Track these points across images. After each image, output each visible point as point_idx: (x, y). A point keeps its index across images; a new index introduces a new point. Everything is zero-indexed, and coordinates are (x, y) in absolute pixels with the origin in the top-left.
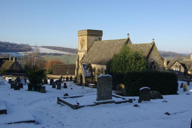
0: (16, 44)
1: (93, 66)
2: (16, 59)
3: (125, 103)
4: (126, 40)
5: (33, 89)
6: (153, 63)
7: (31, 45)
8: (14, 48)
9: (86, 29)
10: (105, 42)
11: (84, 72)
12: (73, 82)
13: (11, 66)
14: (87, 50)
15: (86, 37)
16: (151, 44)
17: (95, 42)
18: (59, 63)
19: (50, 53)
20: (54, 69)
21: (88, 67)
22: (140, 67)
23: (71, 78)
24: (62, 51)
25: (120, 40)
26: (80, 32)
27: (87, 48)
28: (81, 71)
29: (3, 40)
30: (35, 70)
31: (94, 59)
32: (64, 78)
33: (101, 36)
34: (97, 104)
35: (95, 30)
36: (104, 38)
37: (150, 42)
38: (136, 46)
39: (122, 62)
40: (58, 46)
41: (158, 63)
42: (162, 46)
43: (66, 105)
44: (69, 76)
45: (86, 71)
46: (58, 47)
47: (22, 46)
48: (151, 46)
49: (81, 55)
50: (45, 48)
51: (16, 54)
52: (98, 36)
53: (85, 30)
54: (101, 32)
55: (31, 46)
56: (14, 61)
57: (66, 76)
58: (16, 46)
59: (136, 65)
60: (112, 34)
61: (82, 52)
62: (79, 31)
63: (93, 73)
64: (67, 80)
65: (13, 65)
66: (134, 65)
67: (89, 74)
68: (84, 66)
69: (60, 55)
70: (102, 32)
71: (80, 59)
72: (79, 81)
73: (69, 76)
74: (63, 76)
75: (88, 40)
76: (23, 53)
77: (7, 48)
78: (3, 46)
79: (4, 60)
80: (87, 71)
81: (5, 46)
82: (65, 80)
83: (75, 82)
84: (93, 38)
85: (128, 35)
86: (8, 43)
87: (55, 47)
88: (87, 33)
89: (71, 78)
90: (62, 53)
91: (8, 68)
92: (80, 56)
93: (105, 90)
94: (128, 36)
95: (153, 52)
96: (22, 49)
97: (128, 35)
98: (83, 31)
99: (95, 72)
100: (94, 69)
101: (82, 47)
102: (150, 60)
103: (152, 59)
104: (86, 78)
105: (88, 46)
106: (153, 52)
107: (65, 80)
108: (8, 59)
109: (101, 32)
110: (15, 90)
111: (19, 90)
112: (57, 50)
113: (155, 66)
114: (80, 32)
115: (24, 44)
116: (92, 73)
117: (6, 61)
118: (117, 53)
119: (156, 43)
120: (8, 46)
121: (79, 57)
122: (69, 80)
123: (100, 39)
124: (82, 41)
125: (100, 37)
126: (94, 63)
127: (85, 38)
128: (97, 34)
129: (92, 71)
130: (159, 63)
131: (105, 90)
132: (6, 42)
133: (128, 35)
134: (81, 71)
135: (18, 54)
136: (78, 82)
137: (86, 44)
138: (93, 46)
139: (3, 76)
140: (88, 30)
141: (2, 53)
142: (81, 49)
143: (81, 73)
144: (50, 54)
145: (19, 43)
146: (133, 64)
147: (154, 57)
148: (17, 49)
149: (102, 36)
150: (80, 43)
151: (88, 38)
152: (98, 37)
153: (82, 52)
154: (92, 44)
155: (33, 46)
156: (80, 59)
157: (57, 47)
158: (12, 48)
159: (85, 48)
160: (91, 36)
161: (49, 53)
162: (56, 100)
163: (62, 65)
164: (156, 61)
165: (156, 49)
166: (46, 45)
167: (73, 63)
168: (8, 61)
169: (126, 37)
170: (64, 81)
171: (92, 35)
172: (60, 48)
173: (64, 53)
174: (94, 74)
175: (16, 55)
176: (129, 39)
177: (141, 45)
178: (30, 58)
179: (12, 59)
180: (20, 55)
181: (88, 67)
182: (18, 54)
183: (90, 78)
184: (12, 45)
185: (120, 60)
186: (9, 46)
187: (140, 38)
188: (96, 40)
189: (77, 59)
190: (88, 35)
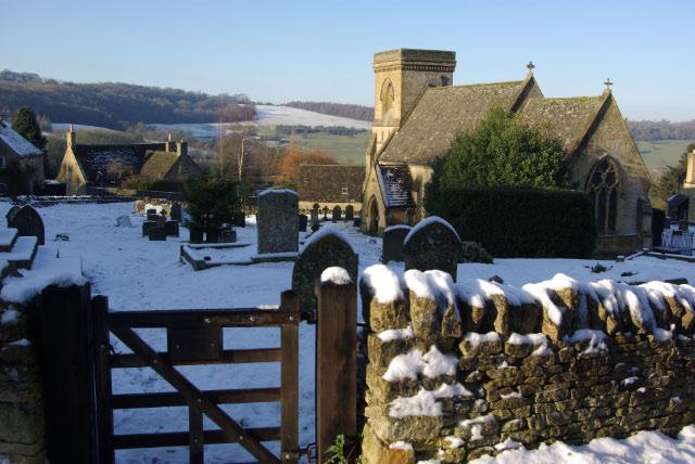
0: (204, 97)
1: (415, 171)
2: (184, 146)
3: (273, 264)
4: (520, 88)
5: (205, 239)
6: (604, 164)
7: (253, 99)
8: (197, 111)
9: (395, 48)
10: (457, 93)
11: (383, 190)
12: (352, 223)
13: (169, 172)
14: (402, 119)
15: (399, 71)
16: (601, 98)
17: (430, 91)
18: (323, 161)
19: (317, 127)
20: (301, 180)
21: (398, 175)
22: (533, 178)
23: (350, 209)
24: (361, 118)
25: (503, 85)
26: (379, 58)
27: (402, 110)
28: (375, 189)
29: (7, 75)
30: (206, 181)
31: (421, 148)
32: (326, 209)
33: (451, 70)
34: (256, 261)
35: (430, 52)
36: (460, 78)
37: (595, 91)
38: (552, 104)
39: (477, 158)
40: (344, 103)
41: (623, 163)
42: (634, 107)
43: (188, 263)
44: (343, 206)
45: (388, 188)
46: (347, 106)
47: (225, 101)
48: (599, 105)
49: (382, 133)
50: (301, 108)
51: (203, 128)
52: (440, 71)
53: (397, 51)
54: (449, 57)
55: (254, 103)
56: (179, 154)
57: (331, 206)
58: (203, 103)
59: (522, 169)
60: (482, 67)
61: (386, 124)
62: (376, 55)
63: (415, 195)
64: (336, 218)
65: (175, 166)
66: (513, 170)
67: (398, 198)
68: (384, 170)
69: (351, 132)
70: (454, 58)
71: (379, 147)
72: (368, 220)
73: (343, 206)
74: (322, 205)
75: (403, 85)
76: (226, 127)
77: (176, 110)
78: (162, 103)
79: (148, 152)
80: (394, 188)
81: (167, 102)
82: (330, 216)
83: (358, 223)
84: (422, 77)
85: (531, 66)
86: (180, 91)
87: (335, 104)
88: (399, 62)
89: (350, 209)
90: (347, 123)
91: (160, 177)
92: (379, 139)
93: (277, 228)
94: (528, 70)
95: (606, 126)
96: (226, 111)
97: (529, 66)
98: (387, 53)
99: (418, 191)
100: (417, 180)
101: (386, 107)
102: (593, 154)
103: (600, 152)
104: (389, 209)
105: (402, 103)
106: (604, 127)
107: (330, 216)
108: (161, 147)
109: (449, 57)
110: (150, 239)
111: (165, 240)
112: (343, 116)
113: (611, 177)
114: (379, 58)
115: (231, 94)
116: (410, 195)
117: (156, 152)
118: (531, 125)
119: (613, 93)
120: (180, 102)
121: (375, 142)
122: (343, 216)
123: (446, 82)
124: (385, 91)
125: (447, 75)
126: (417, 163)
127: (396, 77)
128: (430, 65)
129: (410, 188)
130: (628, 165)
131: (277, 228)
132: (170, 90)
133: (531, 66)
134: (373, 186)
135: (210, 128)
136: (365, 223)
137: (398, 98)
138: (422, 103)
139: (138, 202)
140: (405, 53)
141: (159, 126)
142: (383, 114)
143: (373, 196)
144: (318, 130)
145: (213, 91)
146: (508, 166)
147: (610, 143)
148: (209, 111)
149: (452, 71)
150: (378, 97)
151: (403, 76)
152: (441, 74)
153: (386, 124)
154: (420, 96)
155: (260, 104)
156: (379, 147)
157: (340, 105)
158: (192, 109)
159: (396, 113)
160: (434, 71)
161: (313, 127)
162: (71, 238)
163: (328, 170)
164: (616, 157)
165: (618, 115)
166: (303, 99)
167: (357, 163)
168: (162, 153)
169: (523, 76)
170: (325, 219)
171: (419, 69)
172: (354, 107)
173: (366, 127)
174: (416, 200)
175: (205, 131)
176: (531, 82)
177: (569, 102)
178: (247, 143)
179: (173, 147)
180: (213, 133)
181: (398, 175)
182: (210, 128)
183: (404, 211)
184: (193, 98)
185: (470, 151)
186: (181, 102)
187: (568, 79)
188: (431, 86)
189: (369, 149)
190: (405, 68)
